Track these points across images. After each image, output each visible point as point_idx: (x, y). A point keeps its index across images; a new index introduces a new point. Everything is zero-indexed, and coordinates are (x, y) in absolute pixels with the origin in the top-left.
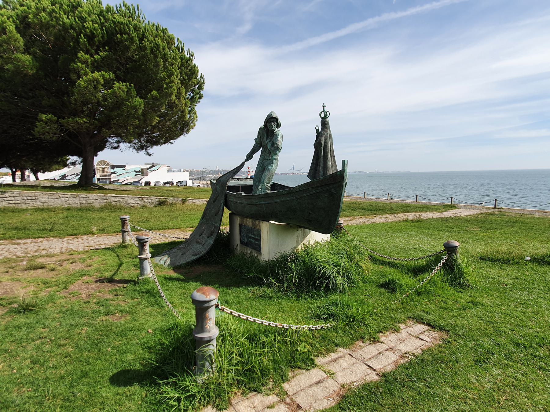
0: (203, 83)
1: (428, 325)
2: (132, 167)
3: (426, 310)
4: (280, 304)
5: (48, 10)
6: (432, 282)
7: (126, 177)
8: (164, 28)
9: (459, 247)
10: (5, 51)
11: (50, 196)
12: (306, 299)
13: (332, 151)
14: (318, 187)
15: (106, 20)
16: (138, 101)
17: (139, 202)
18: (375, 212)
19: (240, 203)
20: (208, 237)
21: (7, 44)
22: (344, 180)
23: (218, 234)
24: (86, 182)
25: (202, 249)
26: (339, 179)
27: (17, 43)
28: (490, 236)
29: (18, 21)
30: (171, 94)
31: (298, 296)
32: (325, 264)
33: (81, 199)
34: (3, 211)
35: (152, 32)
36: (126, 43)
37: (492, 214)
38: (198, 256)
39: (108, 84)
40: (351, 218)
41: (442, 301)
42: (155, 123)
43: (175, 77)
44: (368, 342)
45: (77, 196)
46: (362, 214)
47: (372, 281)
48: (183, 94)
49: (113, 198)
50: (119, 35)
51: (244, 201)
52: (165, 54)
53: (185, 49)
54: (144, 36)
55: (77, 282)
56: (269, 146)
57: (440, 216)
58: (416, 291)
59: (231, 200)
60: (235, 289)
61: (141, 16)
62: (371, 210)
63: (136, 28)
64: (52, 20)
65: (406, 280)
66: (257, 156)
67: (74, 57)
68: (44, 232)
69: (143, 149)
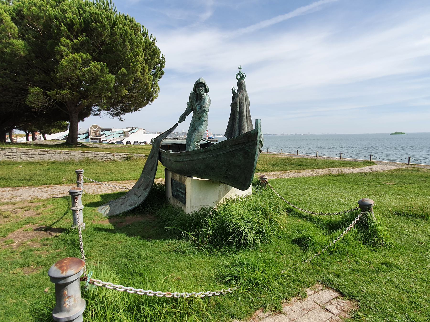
0: (164, 62)
1: (338, 291)
2: (117, 130)
3: (337, 272)
4: (190, 260)
5: (38, 4)
6: (345, 241)
7: (112, 137)
8: (131, 18)
9: (373, 205)
10: (4, 37)
11: (40, 152)
12: (217, 255)
13: (248, 111)
14: (233, 145)
15: (85, 12)
16: (111, 77)
17: (110, 157)
18: (304, 167)
19: (168, 160)
20: (144, 190)
21: (4, 31)
22: (258, 139)
23: (152, 187)
24: (71, 142)
25: (137, 200)
26: (252, 138)
27: (12, 30)
28: (405, 190)
29: (14, 13)
30: (137, 71)
31: (210, 252)
32: (237, 221)
33: (64, 155)
34: (4, 163)
35: (121, 21)
36: (99, 29)
37: (406, 170)
38: (134, 207)
39: (86, 63)
40: (282, 172)
41: (355, 261)
42: (124, 94)
43: (140, 57)
44: (269, 312)
45: (61, 152)
46: (292, 169)
47: (287, 237)
48: (147, 71)
49: (89, 154)
50: (94, 24)
51: (171, 158)
52: (132, 39)
53: (149, 35)
54: (115, 24)
55: (18, 230)
56: (198, 108)
57: (360, 172)
58: (328, 250)
59: (163, 157)
60: (154, 241)
61: (114, 8)
62: (300, 165)
63: (108, 18)
64: (41, 12)
65: (319, 237)
66: (189, 118)
67: (57, 43)
68: (23, 182)
69: (118, 115)
